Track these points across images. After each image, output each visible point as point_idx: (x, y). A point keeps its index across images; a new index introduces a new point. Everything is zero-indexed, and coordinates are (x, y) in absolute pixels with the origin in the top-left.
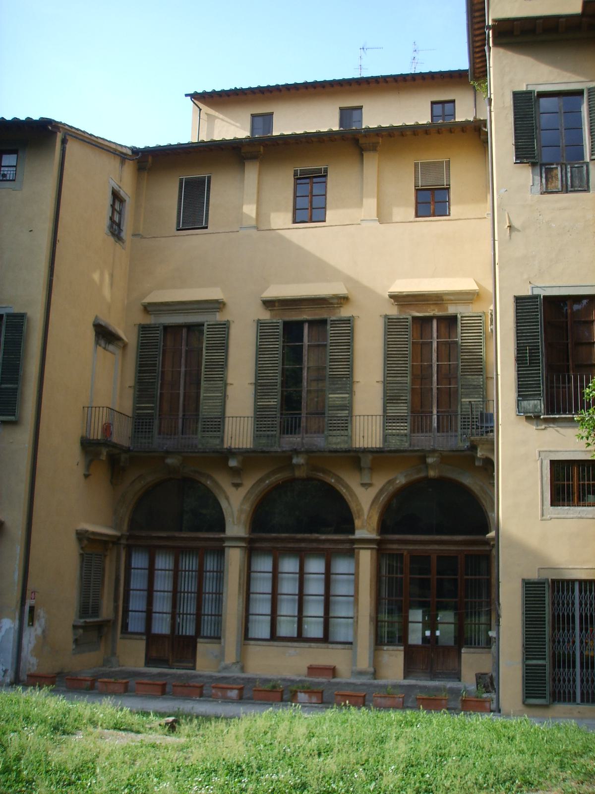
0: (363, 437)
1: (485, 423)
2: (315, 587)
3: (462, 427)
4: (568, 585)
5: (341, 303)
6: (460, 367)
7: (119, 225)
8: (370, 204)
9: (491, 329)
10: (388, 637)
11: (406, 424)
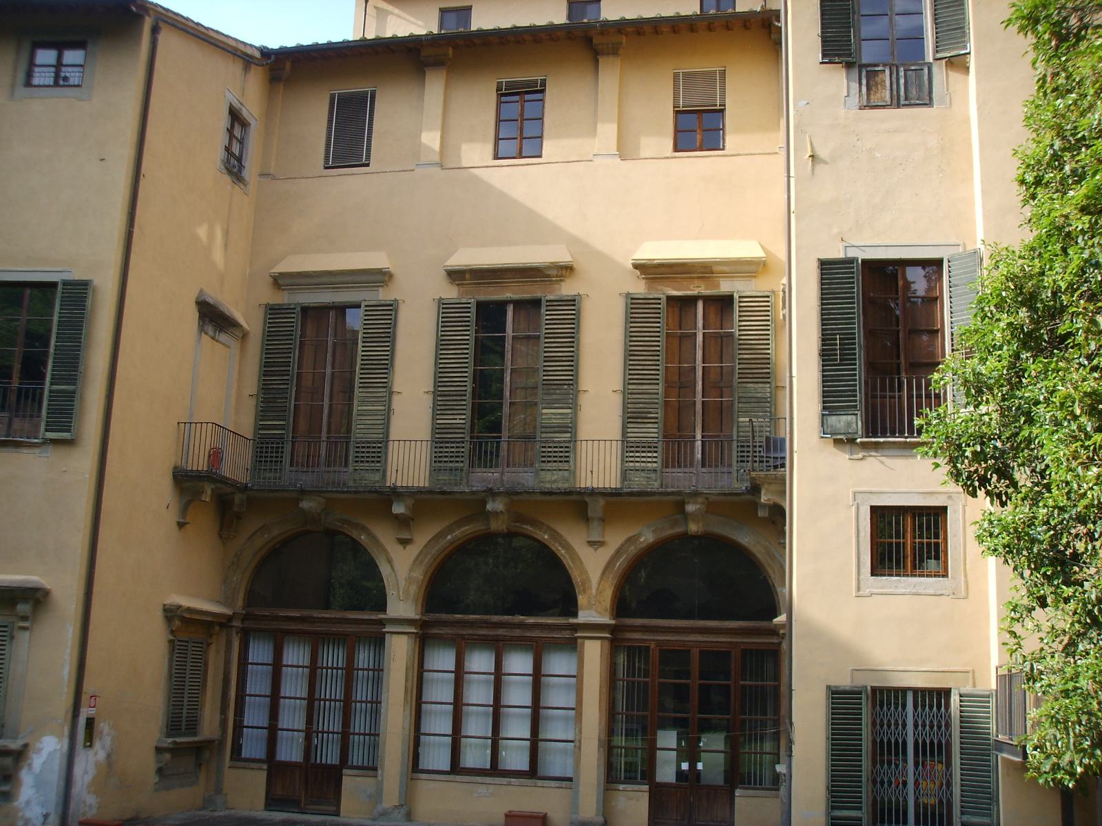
0: (592, 472)
1: (772, 454)
2: (518, 695)
3: (739, 459)
4: (896, 698)
5: (562, 276)
6: (737, 371)
7: (239, 159)
8: (608, 132)
9: (784, 315)
10: (625, 771)
11: (655, 455)
